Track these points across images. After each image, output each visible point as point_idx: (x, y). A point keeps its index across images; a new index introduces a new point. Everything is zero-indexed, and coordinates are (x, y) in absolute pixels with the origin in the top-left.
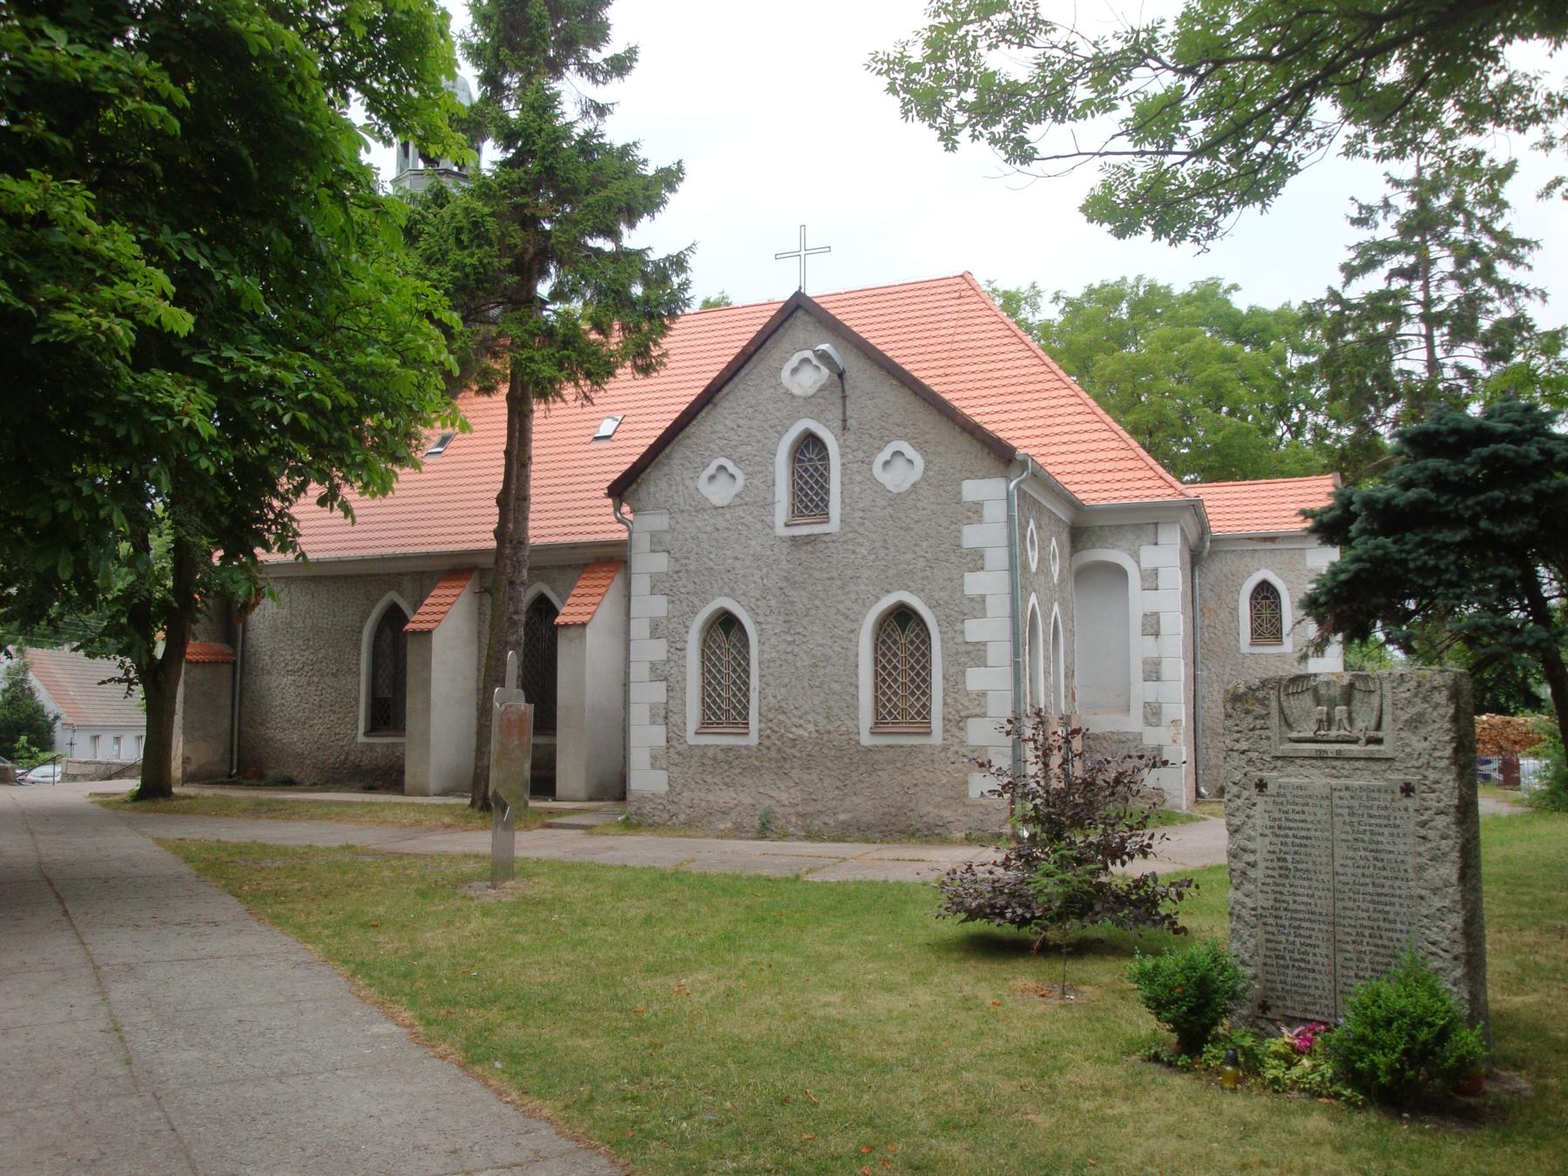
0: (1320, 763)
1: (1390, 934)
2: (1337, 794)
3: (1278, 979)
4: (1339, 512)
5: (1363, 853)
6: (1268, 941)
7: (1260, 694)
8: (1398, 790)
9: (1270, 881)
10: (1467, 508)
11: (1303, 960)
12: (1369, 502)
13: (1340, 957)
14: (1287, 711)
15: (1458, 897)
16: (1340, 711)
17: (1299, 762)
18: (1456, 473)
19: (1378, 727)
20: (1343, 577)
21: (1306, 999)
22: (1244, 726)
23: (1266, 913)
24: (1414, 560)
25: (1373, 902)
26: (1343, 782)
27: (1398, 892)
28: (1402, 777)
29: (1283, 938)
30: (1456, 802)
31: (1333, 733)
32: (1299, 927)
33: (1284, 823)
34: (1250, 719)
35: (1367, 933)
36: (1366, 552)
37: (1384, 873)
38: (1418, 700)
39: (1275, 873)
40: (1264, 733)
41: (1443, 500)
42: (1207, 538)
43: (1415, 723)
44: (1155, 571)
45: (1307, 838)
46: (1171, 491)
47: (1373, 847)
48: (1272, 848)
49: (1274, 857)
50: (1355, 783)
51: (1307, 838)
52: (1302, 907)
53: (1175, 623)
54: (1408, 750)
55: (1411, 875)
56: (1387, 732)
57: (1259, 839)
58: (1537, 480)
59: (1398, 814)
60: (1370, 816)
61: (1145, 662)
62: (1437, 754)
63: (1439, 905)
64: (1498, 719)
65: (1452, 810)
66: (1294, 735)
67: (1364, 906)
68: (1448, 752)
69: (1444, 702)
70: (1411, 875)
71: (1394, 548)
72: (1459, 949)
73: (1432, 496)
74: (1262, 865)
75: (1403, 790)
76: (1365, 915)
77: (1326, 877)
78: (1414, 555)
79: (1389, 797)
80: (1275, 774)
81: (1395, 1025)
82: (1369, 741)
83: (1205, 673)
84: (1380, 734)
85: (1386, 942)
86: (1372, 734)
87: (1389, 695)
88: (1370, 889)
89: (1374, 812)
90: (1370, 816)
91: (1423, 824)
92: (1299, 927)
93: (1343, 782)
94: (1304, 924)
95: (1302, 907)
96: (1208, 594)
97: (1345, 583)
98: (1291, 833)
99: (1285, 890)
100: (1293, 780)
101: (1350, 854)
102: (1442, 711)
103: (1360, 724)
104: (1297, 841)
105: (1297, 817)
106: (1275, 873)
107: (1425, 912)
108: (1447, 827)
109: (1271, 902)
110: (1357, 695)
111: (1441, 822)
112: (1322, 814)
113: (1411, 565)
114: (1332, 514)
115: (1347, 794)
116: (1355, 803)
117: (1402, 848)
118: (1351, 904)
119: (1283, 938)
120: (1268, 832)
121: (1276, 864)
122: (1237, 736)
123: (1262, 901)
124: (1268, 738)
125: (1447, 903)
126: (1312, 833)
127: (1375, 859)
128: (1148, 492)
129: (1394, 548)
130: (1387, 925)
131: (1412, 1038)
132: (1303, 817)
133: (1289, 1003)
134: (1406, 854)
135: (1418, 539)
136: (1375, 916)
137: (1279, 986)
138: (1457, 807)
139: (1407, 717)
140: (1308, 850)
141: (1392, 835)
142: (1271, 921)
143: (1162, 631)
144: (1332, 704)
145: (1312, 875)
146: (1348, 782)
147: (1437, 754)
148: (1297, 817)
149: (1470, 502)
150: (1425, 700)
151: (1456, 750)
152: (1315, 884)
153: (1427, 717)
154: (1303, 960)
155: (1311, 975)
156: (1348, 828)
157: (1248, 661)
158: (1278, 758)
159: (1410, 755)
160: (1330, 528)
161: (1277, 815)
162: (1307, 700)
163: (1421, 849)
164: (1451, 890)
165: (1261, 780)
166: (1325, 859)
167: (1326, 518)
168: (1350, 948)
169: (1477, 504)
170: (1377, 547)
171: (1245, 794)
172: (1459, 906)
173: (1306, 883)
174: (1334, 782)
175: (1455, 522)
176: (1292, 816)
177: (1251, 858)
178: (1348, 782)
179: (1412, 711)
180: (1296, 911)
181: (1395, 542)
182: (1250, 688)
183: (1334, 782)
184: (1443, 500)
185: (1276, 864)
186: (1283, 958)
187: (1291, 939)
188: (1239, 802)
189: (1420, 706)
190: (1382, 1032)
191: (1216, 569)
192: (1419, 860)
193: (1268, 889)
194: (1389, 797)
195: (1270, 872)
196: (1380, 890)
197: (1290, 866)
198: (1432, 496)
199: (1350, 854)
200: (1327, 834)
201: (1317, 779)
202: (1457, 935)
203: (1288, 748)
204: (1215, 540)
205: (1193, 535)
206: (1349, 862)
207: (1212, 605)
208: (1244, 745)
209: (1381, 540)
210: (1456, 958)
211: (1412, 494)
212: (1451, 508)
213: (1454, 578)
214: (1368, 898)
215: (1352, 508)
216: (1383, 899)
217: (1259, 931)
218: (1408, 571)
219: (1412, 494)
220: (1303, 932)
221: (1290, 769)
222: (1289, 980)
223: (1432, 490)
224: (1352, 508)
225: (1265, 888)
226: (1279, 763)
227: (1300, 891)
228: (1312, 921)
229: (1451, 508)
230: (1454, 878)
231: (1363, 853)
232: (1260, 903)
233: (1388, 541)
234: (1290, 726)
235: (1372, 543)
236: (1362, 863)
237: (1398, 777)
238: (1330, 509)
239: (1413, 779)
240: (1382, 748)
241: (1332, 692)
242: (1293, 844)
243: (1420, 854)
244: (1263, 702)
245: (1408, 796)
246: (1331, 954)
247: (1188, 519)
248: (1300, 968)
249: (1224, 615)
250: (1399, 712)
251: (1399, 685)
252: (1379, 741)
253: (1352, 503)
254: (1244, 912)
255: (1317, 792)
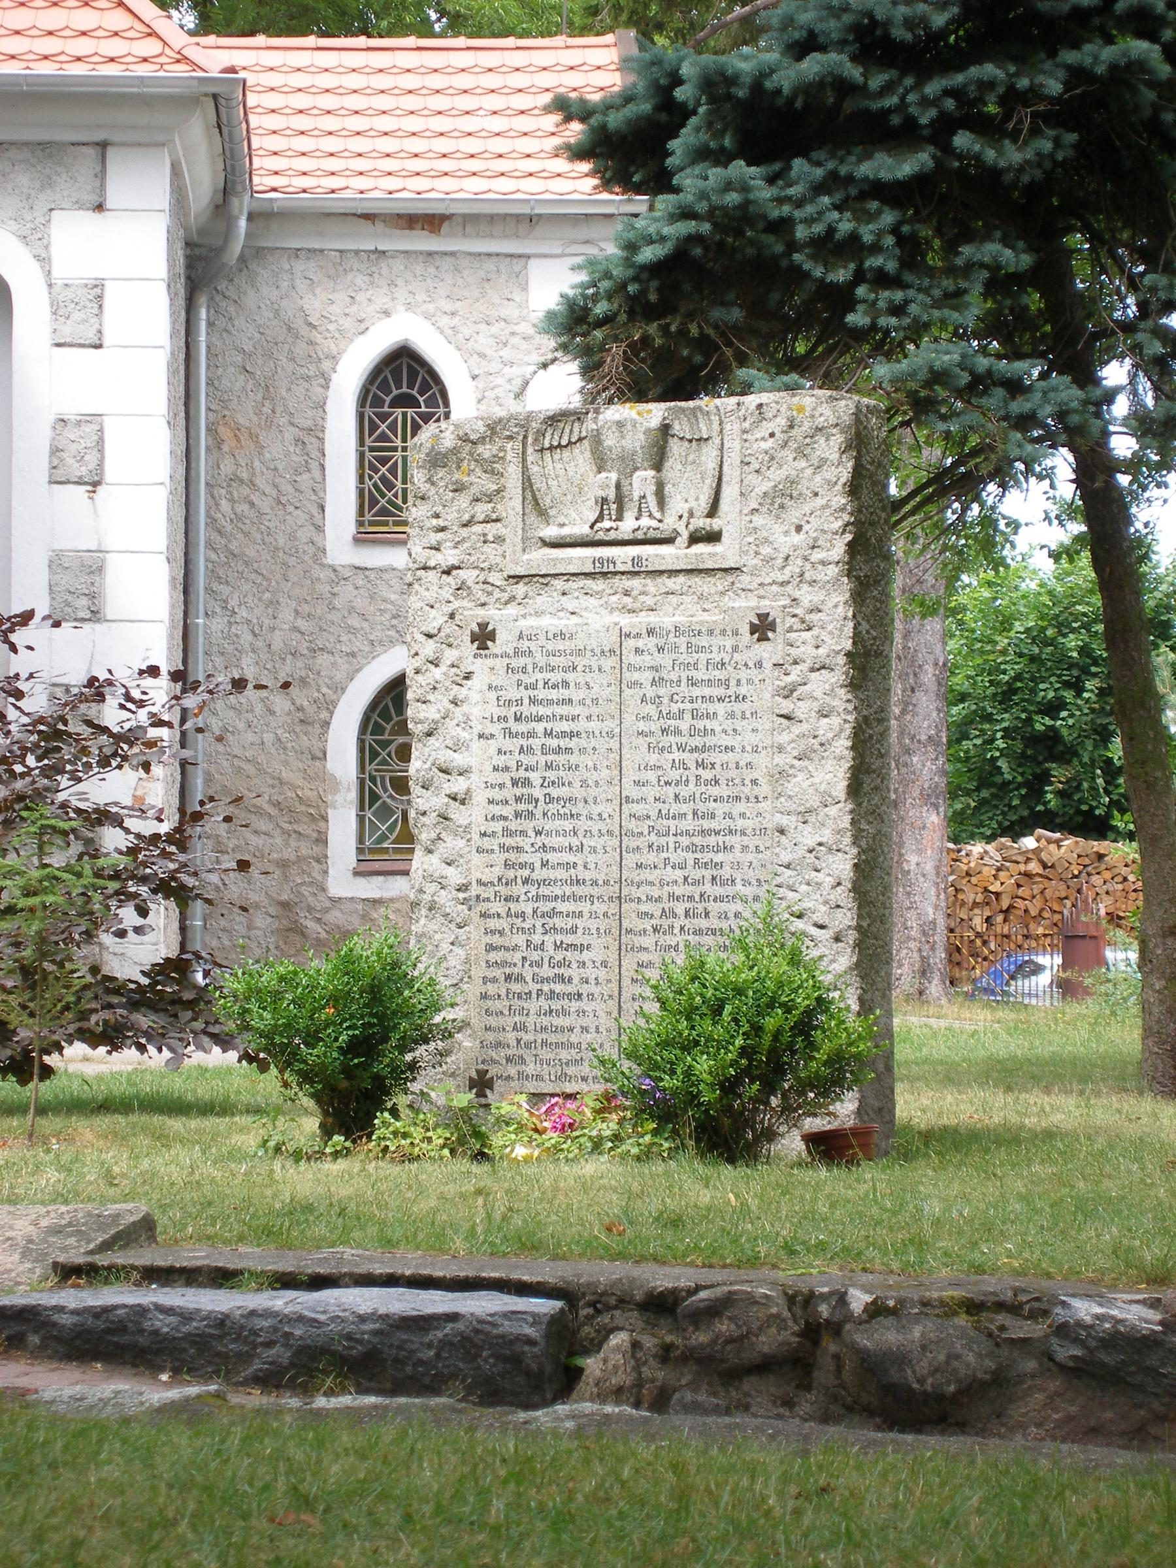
0: (598, 585)
1: (724, 906)
2: (630, 643)
3: (509, 1022)
4: (646, 107)
5: (677, 755)
6: (491, 948)
7: (486, 451)
8: (746, 629)
9: (498, 826)
10: (925, 102)
11: (561, 979)
12: (717, 85)
13: (629, 963)
14: (538, 484)
15: (846, 821)
16: (642, 481)
17: (558, 584)
18: (909, 23)
19: (713, 510)
20: (648, 254)
21: (564, 1055)
22: (450, 517)
23: (489, 893)
24: (809, 221)
25: (692, 848)
26: (645, 619)
27: (740, 824)
28: (753, 602)
29: (520, 939)
30: (848, 645)
31: (628, 526)
32: (554, 913)
33: (526, 709)
34: (463, 501)
35: (680, 909)
36: (703, 195)
37: (715, 791)
38: (789, 454)
39: (507, 811)
40: (492, 530)
41: (876, 82)
42: (242, 207)
43: (781, 498)
44: (97, 292)
45: (572, 735)
46: (150, 47)
47: (697, 741)
48: (501, 761)
49: (506, 778)
50: (665, 619)
51: (572, 735)
52: (560, 874)
53: (143, 452)
54: (766, 550)
55: (764, 789)
56: (728, 520)
57: (477, 745)
58: (1076, 46)
59: (744, 674)
60: (692, 682)
61: (56, 562)
62: (817, 555)
63: (811, 842)
64: (1068, 848)
65: (841, 660)
66: (551, 532)
67: (675, 858)
68: (838, 550)
69: (835, 456)
70: (764, 789)
71: (764, 193)
72: (846, 919)
73: (854, 72)
74: (480, 797)
75: (753, 629)
76: (679, 874)
77: (606, 809)
78: (809, 209)
79: (729, 643)
80: (512, 610)
81: (728, 1008)
82: (695, 538)
83: (218, 624)
84: (716, 524)
85: (715, 923)
86: (700, 522)
87: (737, 445)
88: (689, 824)
89: (700, 675)
90: (692, 682)
91: (788, 692)
92: (554, 913)
93: (645, 619)
94: (562, 907)
95: (560, 874)
96: (232, 380)
97: (656, 269)
98: (540, 727)
99: (525, 843)
100: (546, 622)
101: (653, 759)
102: (830, 473)
103: (677, 504)
104: (553, 743)
105: (554, 694)
106: (507, 811)
107: (785, 857)
108: (830, 693)
109: (498, 870)
110: (675, 448)
111: (820, 684)
112: (601, 686)
113: (801, 233)
114: (631, 111)
115: (650, 643)
116: (665, 660)
117: (750, 739)
118: (651, 858)
119: (520, 939)
120: (495, 729)
121: (509, 793)
122: (435, 538)
123: (479, 868)
124: (499, 540)
125: (827, 835)
126: (581, 725)
127: (700, 764)
128: (82, 46)
129: (764, 193)
130: (718, 890)
131: (757, 1029)
132: (564, 693)
133: (531, 1068)
134: (755, 750)
135: (819, 172)
136: (697, 874)
137: (511, 1037)
138: (848, 654)
139: (766, 486)
140: (574, 759)
141: (731, 715)
142: (497, 907)
143: (110, 475)
144: (629, 467)
145: (580, 808)
146: (653, 619)
147: (817, 555)
148: (554, 694)
149: (932, 88)
150: (801, 453)
151: (851, 545)
152: (583, 825)
153: (802, 487)
154: (561, 979)
155: (575, 1005)
156: (651, 709)
157: (346, 592)
158: (518, 578)
159: (768, 560)
160: (626, 148)
161: (513, 694)
162: (580, 460)
163: (784, 738)
164: (833, 811)
165: (483, 626)
166: (605, 773)
167: (615, 120)
168: (648, 941)
169: (947, 93)
170: (728, 186)
171: (450, 655)
172: (847, 839)
173: (567, 825)
174: (625, 621)
175: (903, 135)
176: (542, 694)
177: (459, 785)
178: (653, 619)
179: (776, 475)
180: (544, 882)
181: (771, 180)
182: (465, 439)
183: (625, 621)
184: (876, 82)
185: (509, 793)
186: (520, 978)
187: (537, 938)
188: (437, 673)
189: (790, 466)
190: (707, 1025)
191: (264, 298)
192: (779, 759)
193: (493, 844)
194: (729, 643)
195: (497, 810)
196: (706, 824)
197: (538, 793)
198: (854, 72)
199: (653, 759)
200: (611, 724)
201: (595, 616)
202: (842, 895)
203: (540, 559)
204: (262, 217)
205: (201, 194)
206: (651, 776)
207: (245, 415)
208: (449, 556)
209: (739, 168)
210: (837, 939)
211: (812, 66)
212: (892, 101)
213: (891, 266)
214: (685, 841)
215: (680, 94)
216: (712, 840)
217: (474, 931)
218: (792, 246)
219: (812, 66)
220: (559, 922)
221: (541, 601)
222: (531, 1020)
223: (854, 59)
224: (680, 94)
225: (486, 843)
226: (520, 589)
227: (556, 841)
228: (575, 898)
229: (892, 101)
230: (840, 788)
231: (677, 755)
232: (476, 875)
233: (752, 173)
234: (543, 513)
235: (716, 174)
236: (674, 775)
237: (746, 606)
238: (628, 98)
239: (772, 606)
240: (718, 548)
241: (627, 443)
242: (544, 750)
243: (780, 749)
244: (491, 467)
245: (763, 638)
246: (613, 958)
247: (196, 136)
248: (552, 995)
249: (279, 447)
250: (752, 479)
251: (757, 424)
252: (713, 537)
253: (678, 81)
254: (444, 897)
255: (593, 644)
